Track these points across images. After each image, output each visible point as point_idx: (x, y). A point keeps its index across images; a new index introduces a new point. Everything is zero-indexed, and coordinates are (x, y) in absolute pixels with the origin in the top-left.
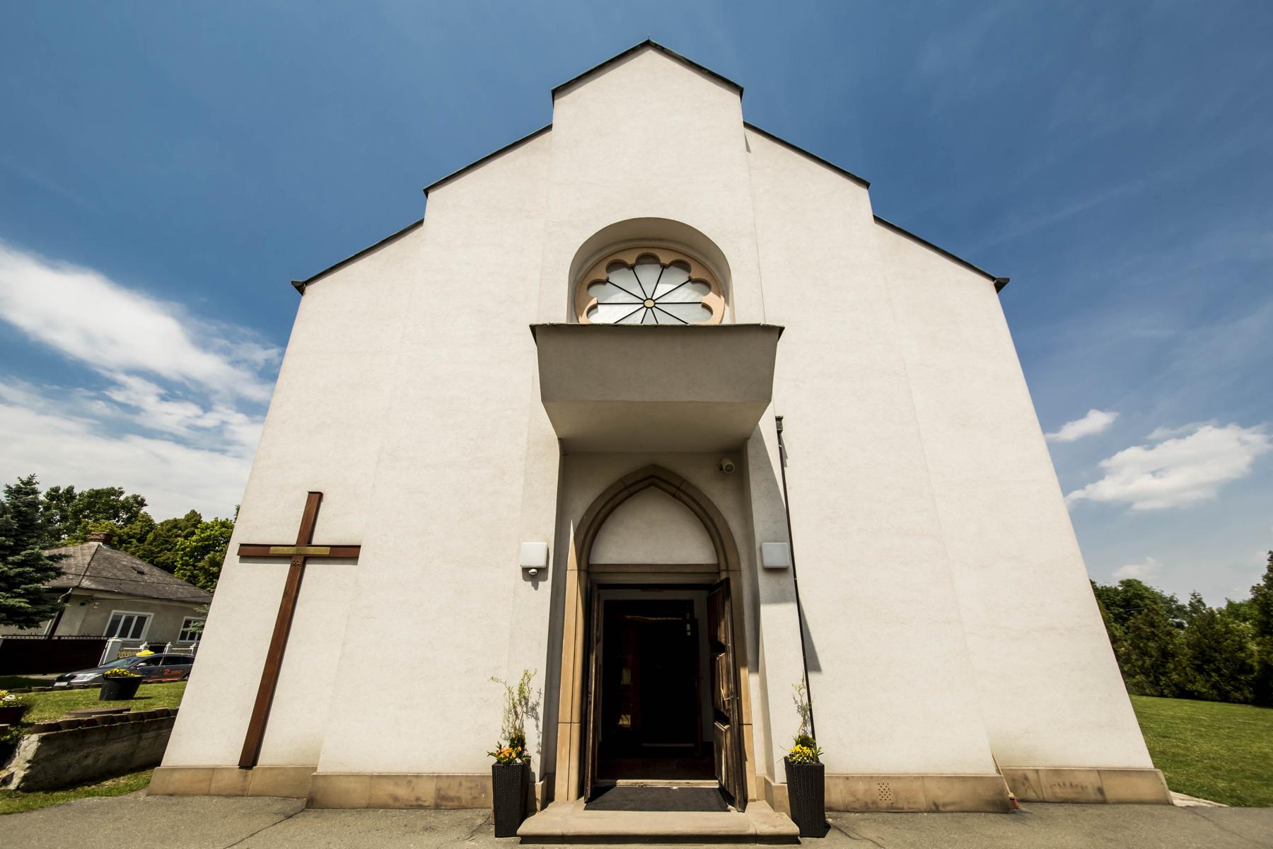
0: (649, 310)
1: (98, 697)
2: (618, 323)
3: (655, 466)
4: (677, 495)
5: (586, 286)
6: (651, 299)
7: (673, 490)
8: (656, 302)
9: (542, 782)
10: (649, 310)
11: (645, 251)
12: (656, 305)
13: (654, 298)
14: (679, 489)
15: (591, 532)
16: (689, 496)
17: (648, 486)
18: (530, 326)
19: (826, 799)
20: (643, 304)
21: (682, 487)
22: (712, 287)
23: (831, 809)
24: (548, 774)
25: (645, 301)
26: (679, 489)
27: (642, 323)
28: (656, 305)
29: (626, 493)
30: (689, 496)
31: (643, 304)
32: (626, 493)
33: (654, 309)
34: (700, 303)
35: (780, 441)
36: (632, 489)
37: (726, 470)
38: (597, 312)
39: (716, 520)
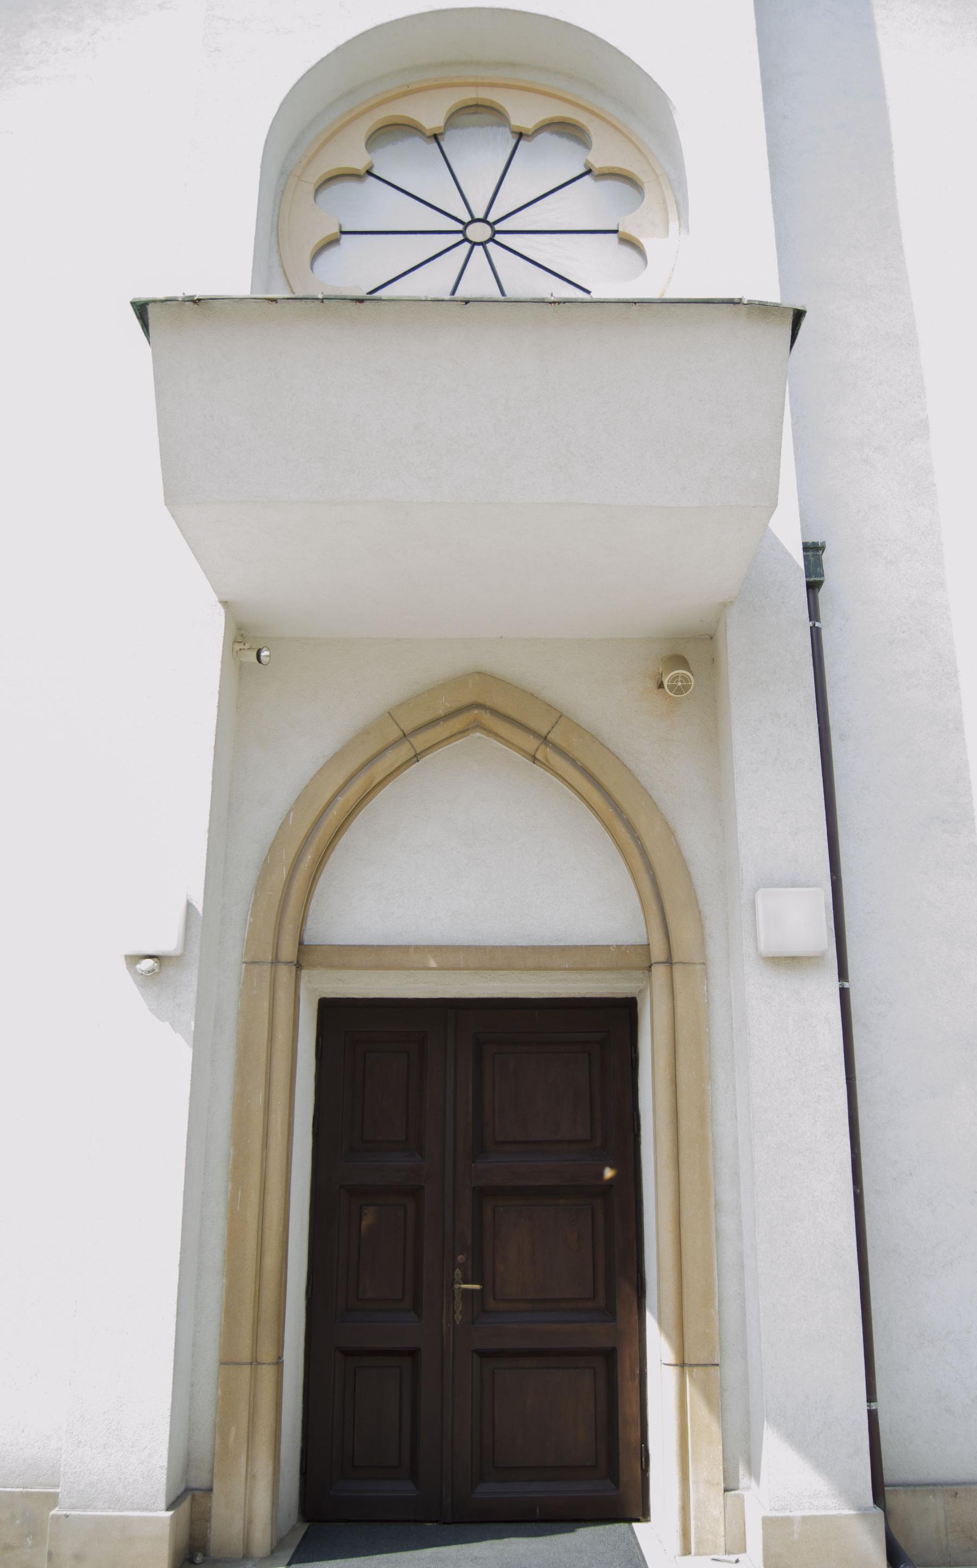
0: (478, 250)
1: (588, 159)
2: (377, 294)
3: (483, 676)
4: (539, 756)
5: (311, 189)
6: (484, 220)
7: (531, 744)
8: (498, 227)
9: (170, 1513)
10: (478, 250)
11: (470, 95)
12: (460, 227)
13: (491, 218)
14: (545, 740)
15: (309, 857)
16: (573, 761)
17: (463, 732)
18: (133, 304)
19: (885, 1481)
20: (462, 232)
21: (554, 737)
22: (647, 187)
23: (888, 1486)
24: (193, 1490)
25: (466, 225)
26: (545, 740)
27: (453, 293)
28: (460, 227)
29: (404, 752)
30: (573, 761)
31: (462, 232)
32: (404, 752)
33: (467, 218)
34: (616, 232)
35: (814, 614)
36: (421, 741)
37: (671, 688)
38: (134, 299)
39: (641, 824)
